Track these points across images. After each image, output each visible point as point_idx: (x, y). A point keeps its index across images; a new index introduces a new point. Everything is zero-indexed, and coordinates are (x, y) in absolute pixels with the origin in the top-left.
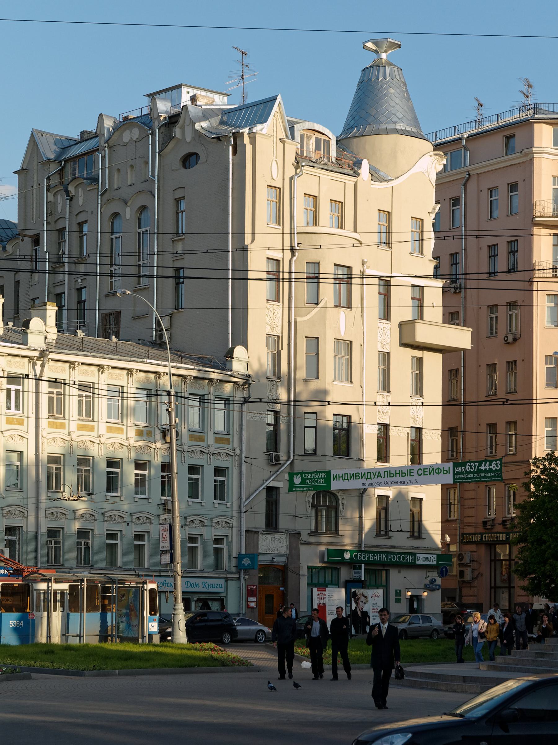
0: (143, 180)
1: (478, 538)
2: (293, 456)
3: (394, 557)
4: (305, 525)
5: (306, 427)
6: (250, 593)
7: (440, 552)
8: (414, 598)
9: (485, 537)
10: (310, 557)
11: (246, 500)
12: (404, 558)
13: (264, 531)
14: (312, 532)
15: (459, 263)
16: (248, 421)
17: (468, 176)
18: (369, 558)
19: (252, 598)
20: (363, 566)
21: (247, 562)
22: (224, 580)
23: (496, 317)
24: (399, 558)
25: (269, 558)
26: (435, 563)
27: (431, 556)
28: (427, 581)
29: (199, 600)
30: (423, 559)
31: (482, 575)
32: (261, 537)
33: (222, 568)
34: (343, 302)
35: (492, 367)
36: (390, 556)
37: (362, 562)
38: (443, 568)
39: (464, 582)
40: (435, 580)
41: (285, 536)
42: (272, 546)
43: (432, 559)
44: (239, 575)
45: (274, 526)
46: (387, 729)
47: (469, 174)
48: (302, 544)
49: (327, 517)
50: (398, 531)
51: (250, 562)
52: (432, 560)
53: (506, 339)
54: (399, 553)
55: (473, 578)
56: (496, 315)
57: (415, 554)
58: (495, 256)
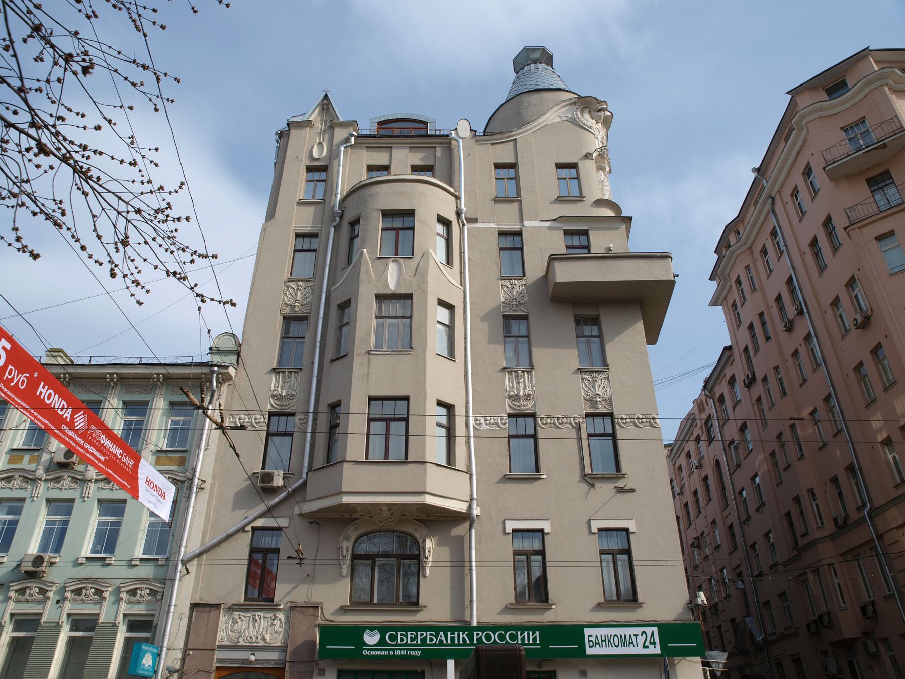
3: (488, 637)
12: (514, 637)
18: (424, 640)
20: (451, 663)
26: (657, 650)
27: (638, 630)
43: (641, 639)
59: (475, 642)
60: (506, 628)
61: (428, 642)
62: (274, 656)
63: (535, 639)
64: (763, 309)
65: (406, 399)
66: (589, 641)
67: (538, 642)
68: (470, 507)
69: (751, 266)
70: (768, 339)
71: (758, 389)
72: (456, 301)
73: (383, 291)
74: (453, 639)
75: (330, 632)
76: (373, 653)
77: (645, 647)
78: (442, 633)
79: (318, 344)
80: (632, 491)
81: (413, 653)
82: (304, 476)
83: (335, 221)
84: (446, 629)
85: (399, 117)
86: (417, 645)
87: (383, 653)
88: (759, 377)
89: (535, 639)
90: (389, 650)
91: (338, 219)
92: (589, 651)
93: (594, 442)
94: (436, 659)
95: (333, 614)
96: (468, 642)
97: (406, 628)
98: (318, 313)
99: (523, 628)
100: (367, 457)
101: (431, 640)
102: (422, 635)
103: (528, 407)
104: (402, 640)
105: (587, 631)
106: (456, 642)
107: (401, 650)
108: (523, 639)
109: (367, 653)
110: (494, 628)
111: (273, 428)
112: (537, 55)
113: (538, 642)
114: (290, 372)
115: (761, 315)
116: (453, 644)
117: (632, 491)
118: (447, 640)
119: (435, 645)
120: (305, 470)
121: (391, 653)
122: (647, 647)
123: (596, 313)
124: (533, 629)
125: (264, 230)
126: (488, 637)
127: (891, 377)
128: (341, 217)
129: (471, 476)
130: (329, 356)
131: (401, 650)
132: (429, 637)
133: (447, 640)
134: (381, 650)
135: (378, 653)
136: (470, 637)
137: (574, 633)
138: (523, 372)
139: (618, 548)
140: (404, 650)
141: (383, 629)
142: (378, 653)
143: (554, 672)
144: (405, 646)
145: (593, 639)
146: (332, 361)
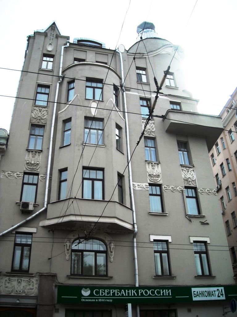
0: (206, 226)
3: (146, 293)
12: (159, 293)
18: (114, 294)
20: (130, 306)
25: (36, 289)
26: (223, 298)
27: (215, 289)
38: (232, 301)
43: (217, 293)
46: (27, 304)
59: (140, 295)
60: (155, 288)
61: (116, 295)
62: (33, 302)
63: (169, 293)
64: (228, 157)
65: (102, 169)
66: (194, 294)
67: (170, 295)
68: (134, 227)
69: (223, 138)
70: (230, 170)
71: (223, 192)
72: (123, 126)
73: (88, 115)
74: (128, 293)
75: (63, 289)
76: (87, 300)
77: (219, 296)
78: (123, 290)
79: (52, 139)
80: (207, 224)
81: (108, 300)
82: (45, 206)
83: (60, 80)
84: (125, 289)
85: (86, 39)
86: (110, 296)
87: (92, 300)
88: (224, 187)
89: (169, 293)
90: (95, 299)
91: (61, 79)
92: (194, 299)
93: (188, 199)
94: (121, 305)
95: (69, 277)
96: (136, 295)
97: (104, 288)
98: (51, 124)
99: (163, 288)
100: (82, 197)
101: (118, 294)
102: (113, 291)
103: (160, 181)
104: (102, 294)
105: (193, 289)
106: (130, 295)
107: (102, 299)
108: (163, 293)
109: (84, 300)
110: (149, 288)
111: (25, 181)
112: (149, 26)
113: (170, 295)
114: (36, 152)
115: (227, 159)
116: (129, 296)
117: (207, 224)
118: (126, 294)
119: (119, 296)
120: (46, 203)
121: (97, 300)
122: (220, 297)
123: (187, 141)
124: (168, 288)
125: (21, 81)
126: (146, 293)
127: (26, 262)
128: (63, 79)
129: (133, 212)
130: (58, 145)
131: (102, 299)
132: (116, 292)
133: (126, 294)
134: (91, 299)
135: (90, 300)
136: (137, 292)
137: (187, 290)
138: (155, 164)
139: (203, 249)
140: (103, 299)
141: (92, 288)
142: (90, 300)
143: (177, 309)
144: (104, 296)
145: (196, 293)
146: (60, 148)
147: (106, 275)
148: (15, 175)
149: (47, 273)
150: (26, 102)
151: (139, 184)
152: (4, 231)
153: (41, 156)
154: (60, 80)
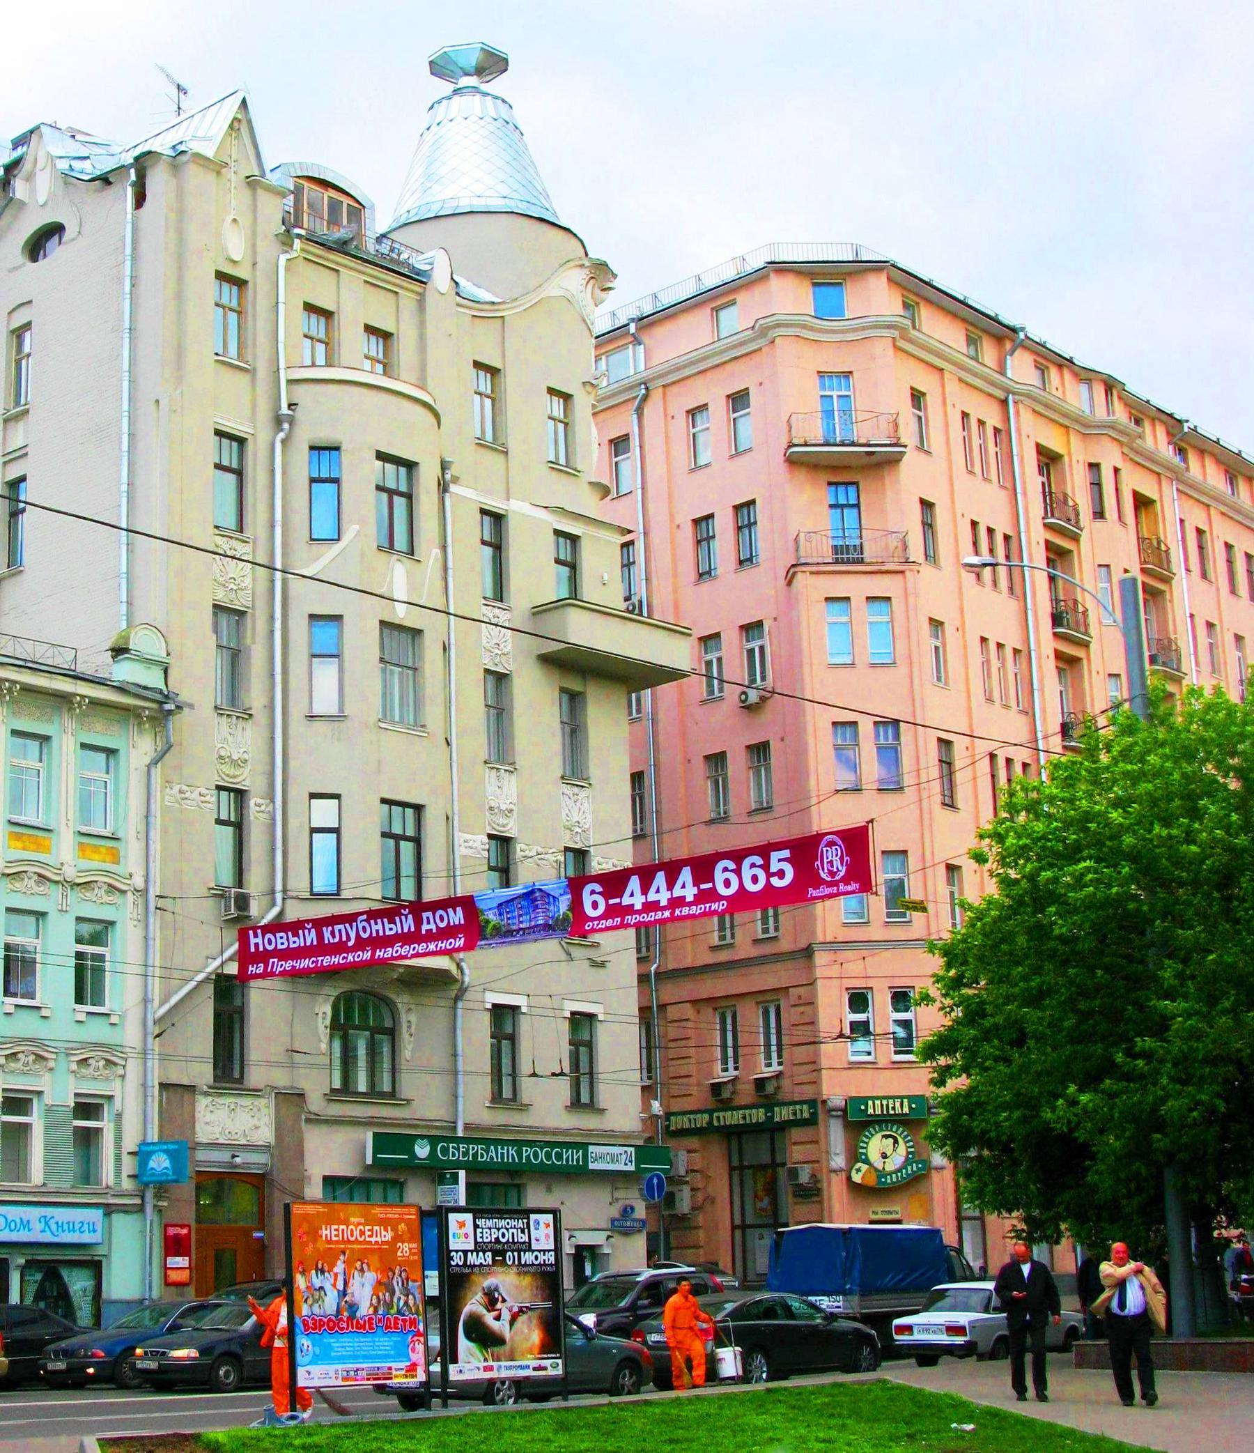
1: (702, 1120)
2: (284, 899)
3: (536, 1155)
4: (317, 1083)
5: (314, 830)
6: (174, 1246)
7: (641, 1143)
8: (585, 1254)
9: (718, 1118)
10: (332, 1152)
11: (161, 1005)
13: (210, 1087)
14: (333, 1091)
15: (634, 563)
16: (166, 810)
17: (643, 391)
18: (475, 1155)
19: (179, 1259)
20: (462, 1174)
21: (160, 1163)
22: (101, 1211)
23: (719, 660)
24: (548, 1156)
26: (631, 1167)
27: (622, 1149)
28: (614, 1211)
29: (30, 1265)
30: (604, 1158)
31: (713, 1201)
32: (202, 1102)
33: (98, 1182)
34: (401, 541)
35: (717, 760)
36: (527, 1151)
37: (459, 1165)
38: (651, 1179)
39: (675, 1217)
40: (632, 1208)
41: (263, 1101)
42: (234, 1126)
43: (624, 1157)
44: (143, 1198)
45: (236, 1075)
47: (647, 389)
48: (308, 1120)
49: (401, 682)
50: (554, 1074)
51: (167, 1164)
52: (622, 1160)
53: (743, 697)
54: (548, 1144)
55: (693, 1209)
56: (718, 655)
57: (584, 1146)
58: (710, 538)
62: (261, 1158)
104: (454, 1155)
143: (525, 1185)
147: (393, 1094)
148: (195, 795)
149: (285, 1088)
150: (971, 1426)
151: (468, 837)
152: (941, 1283)
153: (248, 732)
154: (282, 430)
